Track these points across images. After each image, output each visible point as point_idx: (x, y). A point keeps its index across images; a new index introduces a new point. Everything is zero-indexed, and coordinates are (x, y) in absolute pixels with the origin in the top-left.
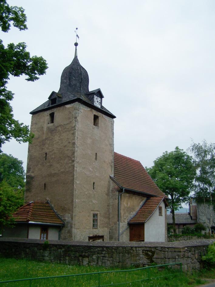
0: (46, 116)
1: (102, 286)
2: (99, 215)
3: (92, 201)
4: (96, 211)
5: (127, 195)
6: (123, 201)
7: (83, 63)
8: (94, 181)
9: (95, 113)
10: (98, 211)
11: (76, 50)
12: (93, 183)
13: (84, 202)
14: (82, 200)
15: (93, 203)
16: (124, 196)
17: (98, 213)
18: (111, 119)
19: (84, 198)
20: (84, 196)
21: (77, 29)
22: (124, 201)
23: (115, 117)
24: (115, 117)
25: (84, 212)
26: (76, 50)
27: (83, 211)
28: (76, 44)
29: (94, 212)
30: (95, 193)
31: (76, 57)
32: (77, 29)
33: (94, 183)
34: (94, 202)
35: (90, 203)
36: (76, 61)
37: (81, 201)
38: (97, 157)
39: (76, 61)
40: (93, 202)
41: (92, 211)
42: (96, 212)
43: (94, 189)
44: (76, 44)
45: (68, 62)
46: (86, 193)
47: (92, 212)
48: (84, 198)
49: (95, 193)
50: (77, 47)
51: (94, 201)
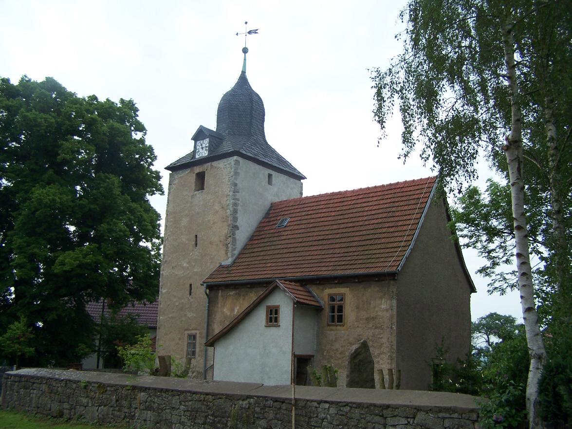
0: (189, 177)
1: (394, 426)
2: (198, 336)
3: (185, 315)
4: (192, 330)
5: (232, 293)
6: (219, 306)
7: (256, 85)
8: (191, 281)
9: (268, 171)
10: (196, 329)
11: (245, 60)
12: (189, 285)
13: (172, 318)
14: (170, 316)
15: (188, 317)
16: (222, 296)
17: (196, 333)
18: (297, 181)
19: (173, 312)
20: (173, 309)
21: (246, 23)
22: (223, 306)
23: (304, 178)
24: (304, 178)
25: (172, 333)
26: (245, 60)
27: (171, 332)
28: (245, 51)
29: (190, 332)
30: (192, 300)
31: (243, 73)
32: (246, 23)
33: (191, 285)
34: (190, 316)
35: (183, 319)
36: (243, 80)
37: (169, 317)
38: (194, 239)
39: (243, 80)
40: (188, 315)
41: (185, 330)
42: (194, 332)
43: (190, 294)
44: (245, 51)
45: (229, 83)
46: (177, 304)
47: (186, 332)
48: (173, 312)
49: (192, 300)
50: (246, 54)
51: (190, 315)
